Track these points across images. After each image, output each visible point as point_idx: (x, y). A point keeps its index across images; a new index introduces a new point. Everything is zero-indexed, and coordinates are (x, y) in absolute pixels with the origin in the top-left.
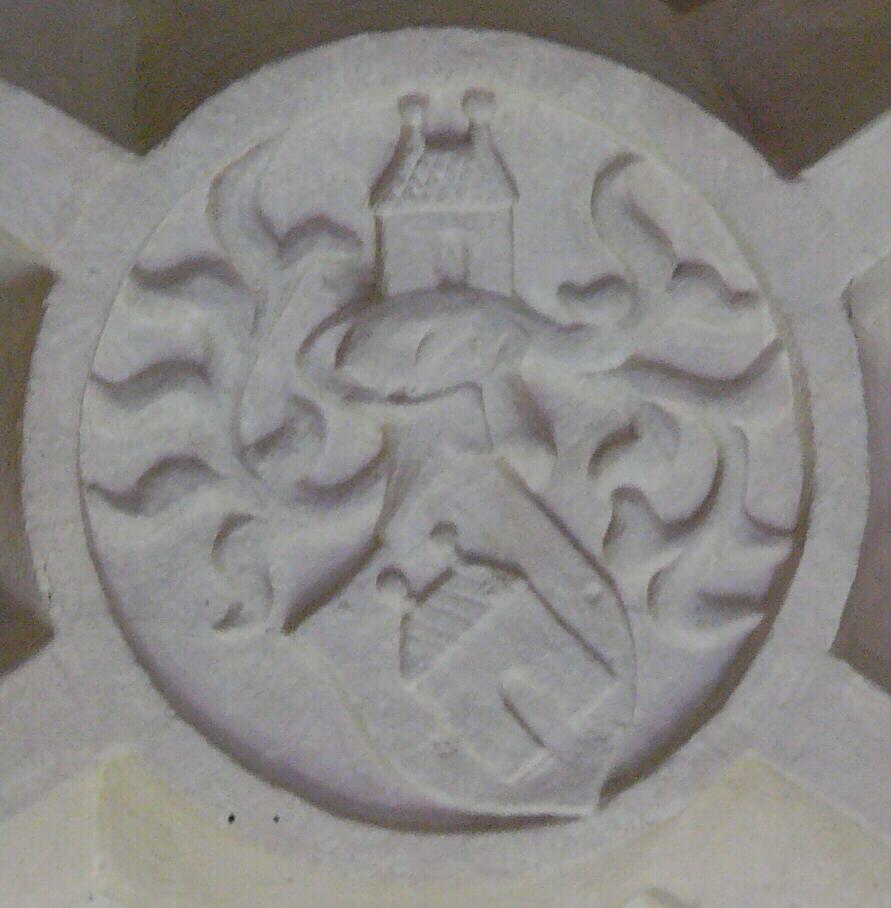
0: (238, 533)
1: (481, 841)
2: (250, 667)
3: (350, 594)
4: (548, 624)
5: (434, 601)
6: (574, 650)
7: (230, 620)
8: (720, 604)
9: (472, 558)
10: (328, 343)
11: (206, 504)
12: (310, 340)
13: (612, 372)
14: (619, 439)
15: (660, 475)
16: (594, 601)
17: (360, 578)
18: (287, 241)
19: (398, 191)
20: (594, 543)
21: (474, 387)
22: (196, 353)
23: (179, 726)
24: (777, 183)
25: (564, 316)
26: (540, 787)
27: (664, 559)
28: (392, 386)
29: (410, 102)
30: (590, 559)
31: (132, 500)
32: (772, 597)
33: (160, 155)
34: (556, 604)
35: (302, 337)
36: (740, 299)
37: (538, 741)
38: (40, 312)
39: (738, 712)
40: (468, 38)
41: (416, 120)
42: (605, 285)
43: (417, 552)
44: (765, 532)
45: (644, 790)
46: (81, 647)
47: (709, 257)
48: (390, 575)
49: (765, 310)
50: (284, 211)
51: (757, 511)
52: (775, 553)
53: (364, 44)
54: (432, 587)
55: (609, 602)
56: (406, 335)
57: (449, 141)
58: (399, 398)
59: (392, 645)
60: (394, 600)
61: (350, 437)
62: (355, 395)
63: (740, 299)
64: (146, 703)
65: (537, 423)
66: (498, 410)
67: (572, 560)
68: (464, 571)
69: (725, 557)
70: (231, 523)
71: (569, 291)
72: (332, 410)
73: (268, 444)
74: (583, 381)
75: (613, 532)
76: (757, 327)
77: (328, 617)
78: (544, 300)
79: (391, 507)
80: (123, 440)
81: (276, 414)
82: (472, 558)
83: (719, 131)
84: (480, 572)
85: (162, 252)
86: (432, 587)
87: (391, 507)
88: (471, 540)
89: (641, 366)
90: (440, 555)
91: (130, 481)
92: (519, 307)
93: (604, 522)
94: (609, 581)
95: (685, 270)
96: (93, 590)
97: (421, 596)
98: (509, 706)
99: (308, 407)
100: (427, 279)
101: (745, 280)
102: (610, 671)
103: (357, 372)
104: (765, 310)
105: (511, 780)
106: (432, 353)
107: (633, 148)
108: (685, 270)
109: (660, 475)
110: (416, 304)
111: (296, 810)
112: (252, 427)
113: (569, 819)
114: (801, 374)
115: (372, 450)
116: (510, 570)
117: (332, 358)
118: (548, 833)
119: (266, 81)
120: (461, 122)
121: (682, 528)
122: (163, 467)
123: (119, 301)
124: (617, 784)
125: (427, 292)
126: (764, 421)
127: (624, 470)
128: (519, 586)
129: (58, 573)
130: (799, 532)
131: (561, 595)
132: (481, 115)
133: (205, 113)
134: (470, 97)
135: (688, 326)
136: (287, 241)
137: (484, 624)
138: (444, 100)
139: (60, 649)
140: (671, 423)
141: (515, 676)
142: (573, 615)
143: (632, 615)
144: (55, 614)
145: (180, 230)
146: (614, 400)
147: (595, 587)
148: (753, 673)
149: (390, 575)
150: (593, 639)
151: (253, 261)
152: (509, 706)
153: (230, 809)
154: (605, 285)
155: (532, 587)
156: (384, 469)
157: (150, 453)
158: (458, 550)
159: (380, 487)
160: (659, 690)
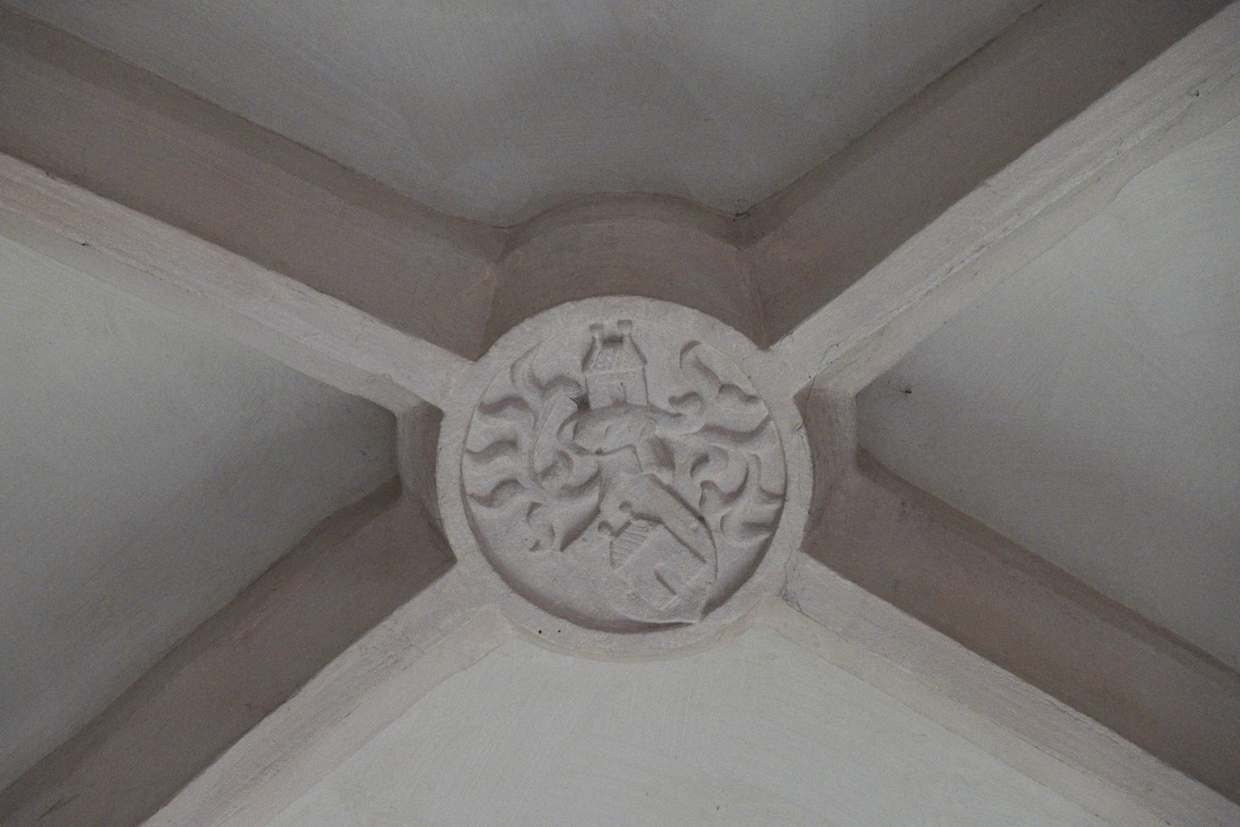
0: (535, 512)
2: (542, 567)
3: (586, 534)
4: (673, 542)
5: (623, 536)
6: (686, 553)
7: (536, 546)
8: (752, 527)
9: (640, 516)
10: (569, 429)
11: (520, 500)
12: (561, 428)
13: (696, 434)
14: (702, 460)
16: (695, 531)
17: (590, 527)
18: (544, 388)
19: (591, 366)
20: (695, 504)
21: (631, 446)
22: (511, 437)
25: (673, 410)
26: (676, 611)
27: (724, 512)
28: (595, 448)
29: (592, 328)
31: (489, 501)
32: (771, 526)
33: (483, 360)
34: (678, 533)
35: (558, 426)
36: (751, 399)
37: (673, 592)
38: (439, 427)
39: (759, 578)
41: (597, 336)
42: (691, 396)
44: (771, 497)
45: (719, 611)
47: (737, 383)
48: (604, 525)
49: (762, 403)
50: (544, 375)
51: (765, 487)
52: (774, 506)
53: (569, 306)
54: (622, 530)
55: (702, 530)
56: (601, 427)
57: (613, 341)
58: (599, 453)
59: (606, 555)
60: (606, 537)
61: (583, 467)
62: (581, 451)
63: (751, 399)
65: (665, 454)
66: (645, 455)
67: (685, 514)
68: (635, 523)
69: (750, 507)
70: (534, 506)
71: (673, 400)
72: (575, 458)
73: (548, 472)
74: (685, 435)
75: (703, 500)
76: (757, 412)
77: (578, 545)
78: (663, 404)
79: (602, 496)
80: (482, 477)
81: (550, 458)
82: (640, 516)
83: (731, 332)
84: (642, 523)
85: (492, 396)
86: (622, 530)
87: (602, 496)
88: (638, 507)
89: (709, 429)
90: (624, 516)
91: (488, 492)
92: (652, 409)
93: (698, 496)
94: (702, 519)
95: (725, 388)
96: (472, 541)
97: (617, 534)
98: (660, 579)
99: (564, 455)
100: (608, 401)
101: (752, 392)
102: (704, 561)
104: (762, 403)
106: (614, 436)
108: (725, 388)
109: (723, 475)
110: (603, 413)
112: (539, 465)
113: (688, 624)
115: (595, 470)
116: (659, 521)
117: (571, 434)
118: (679, 631)
119: (528, 325)
120: (618, 332)
121: (734, 496)
122: (503, 484)
123: (475, 418)
124: (711, 606)
125: (609, 407)
126: (764, 449)
127: (704, 474)
128: (660, 528)
130: (783, 497)
131: (680, 529)
132: (626, 331)
133: (501, 341)
134: (620, 323)
135: (727, 411)
136: (544, 388)
137: (645, 544)
138: (610, 325)
139: (459, 567)
140: (724, 454)
141: (660, 565)
142: (686, 538)
143: (714, 534)
146: (699, 444)
147: (696, 524)
148: (765, 560)
149: (604, 525)
150: (694, 547)
151: (531, 397)
152: (660, 579)
154: (691, 396)
155: (666, 527)
157: (496, 479)
158: (632, 513)
159: (597, 488)
160: (728, 565)
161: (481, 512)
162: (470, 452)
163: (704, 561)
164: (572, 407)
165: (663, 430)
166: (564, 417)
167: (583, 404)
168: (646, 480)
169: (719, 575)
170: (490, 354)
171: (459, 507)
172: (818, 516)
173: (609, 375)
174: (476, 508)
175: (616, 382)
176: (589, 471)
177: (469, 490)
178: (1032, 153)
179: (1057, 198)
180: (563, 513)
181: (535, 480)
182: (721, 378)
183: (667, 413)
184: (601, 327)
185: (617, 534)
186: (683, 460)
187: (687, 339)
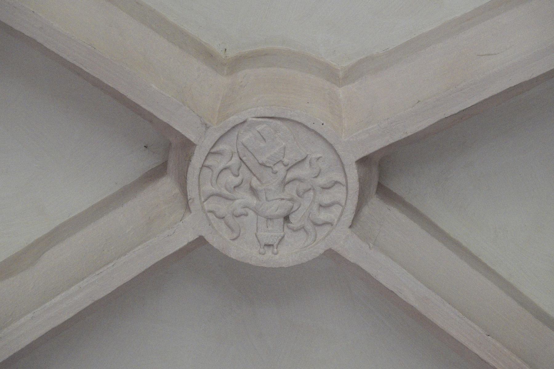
1: (273, 115)
3: (295, 162)
5: (278, 160)
6: (250, 149)
11: (322, 181)
15: (230, 179)
16: (245, 156)
20: (243, 166)
23: (332, 143)
24: (203, 235)
25: (247, 209)
27: (230, 163)
28: (283, 202)
30: (244, 163)
39: (218, 135)
40: (264, 265)
41: (275, 250)
43: (280, 168)
44: (209, 167)
45: (238, 122)
46: (351, 159)
47: (217, 219)
48: (285, 166)
50: (302, 234)
55: (241, 156)
58: (282, 199)
60: (286, 161)
61: (291, 191)
64: (339, 148)
65: (253, 191)
67: (249, 164)
68: (272, 165)
69: (218, 163)
71: (246, 215)
72: (294, 194)
74: (244, 198)
77: (299, 159)
78: (251, 213)
79: (285, 177)
80: (338, 194)
81: (306, 195)
84: (268, 165)
90: (276, 169)
92: (257, 213)
96: (347, 170)
98: (264, 139)
101: (209, 214)
103: (290, 204)
105: (265, 125)
106: (276, 207)
107: (231, 242)
110: (278, 217)
111: (309, 125)
112: (311, 193)
114: (200, 199)
115: (286, 186)
116: (262, 165)
118: (259, 115)
126: (208, 188)
127: (237, 180)
128: (260, 162)
129: (353, 174)
132: (262, 250)
135: (223, 208)
141: (262, 145)
143: (236, 152)
144: (354, 166)
145: (323, 232)
147: (244, 159)
151: (309, 227)
152: (264, 139)
153: (323, 122)
156: (285, 183)
158: (272, 169)
159: (287, 180)
161: (339, 177)
162: (341, 205)
163: (243, 144)
164: (292, 218)
165: (253, 201)
166: (296, 212)
167: (286, 218)
168: (264, 182)
169: (237, 133)
170: (323, 251)
171: (350, 181)
172: (188, 159)
173: (272, 232)
174: (343, 181)
175: (270, 228)
176: (288, 187)
177: (345, 188)
178: (71, 315)
179: (63, 294)
180: (303, 172)
181: (314, 189)
182: (223, 222)
183: (250, 209)
184: (273, 253)
185: (281, 161)
186: (246, 186)
187: (236, 242)
